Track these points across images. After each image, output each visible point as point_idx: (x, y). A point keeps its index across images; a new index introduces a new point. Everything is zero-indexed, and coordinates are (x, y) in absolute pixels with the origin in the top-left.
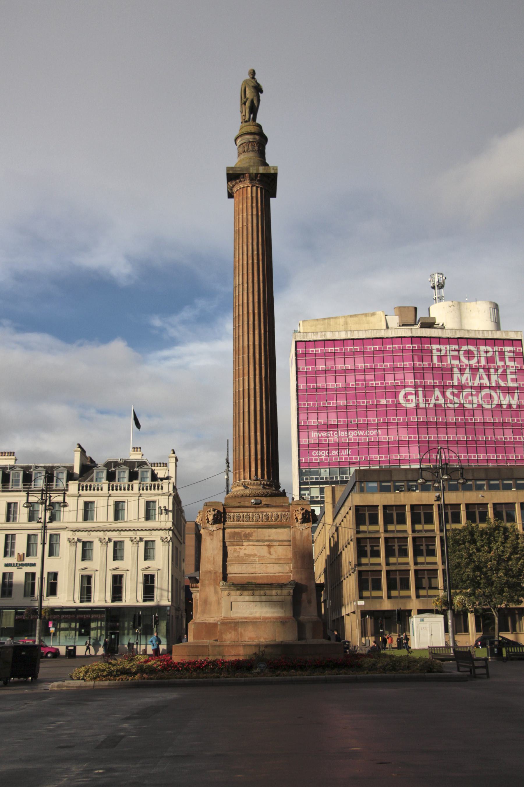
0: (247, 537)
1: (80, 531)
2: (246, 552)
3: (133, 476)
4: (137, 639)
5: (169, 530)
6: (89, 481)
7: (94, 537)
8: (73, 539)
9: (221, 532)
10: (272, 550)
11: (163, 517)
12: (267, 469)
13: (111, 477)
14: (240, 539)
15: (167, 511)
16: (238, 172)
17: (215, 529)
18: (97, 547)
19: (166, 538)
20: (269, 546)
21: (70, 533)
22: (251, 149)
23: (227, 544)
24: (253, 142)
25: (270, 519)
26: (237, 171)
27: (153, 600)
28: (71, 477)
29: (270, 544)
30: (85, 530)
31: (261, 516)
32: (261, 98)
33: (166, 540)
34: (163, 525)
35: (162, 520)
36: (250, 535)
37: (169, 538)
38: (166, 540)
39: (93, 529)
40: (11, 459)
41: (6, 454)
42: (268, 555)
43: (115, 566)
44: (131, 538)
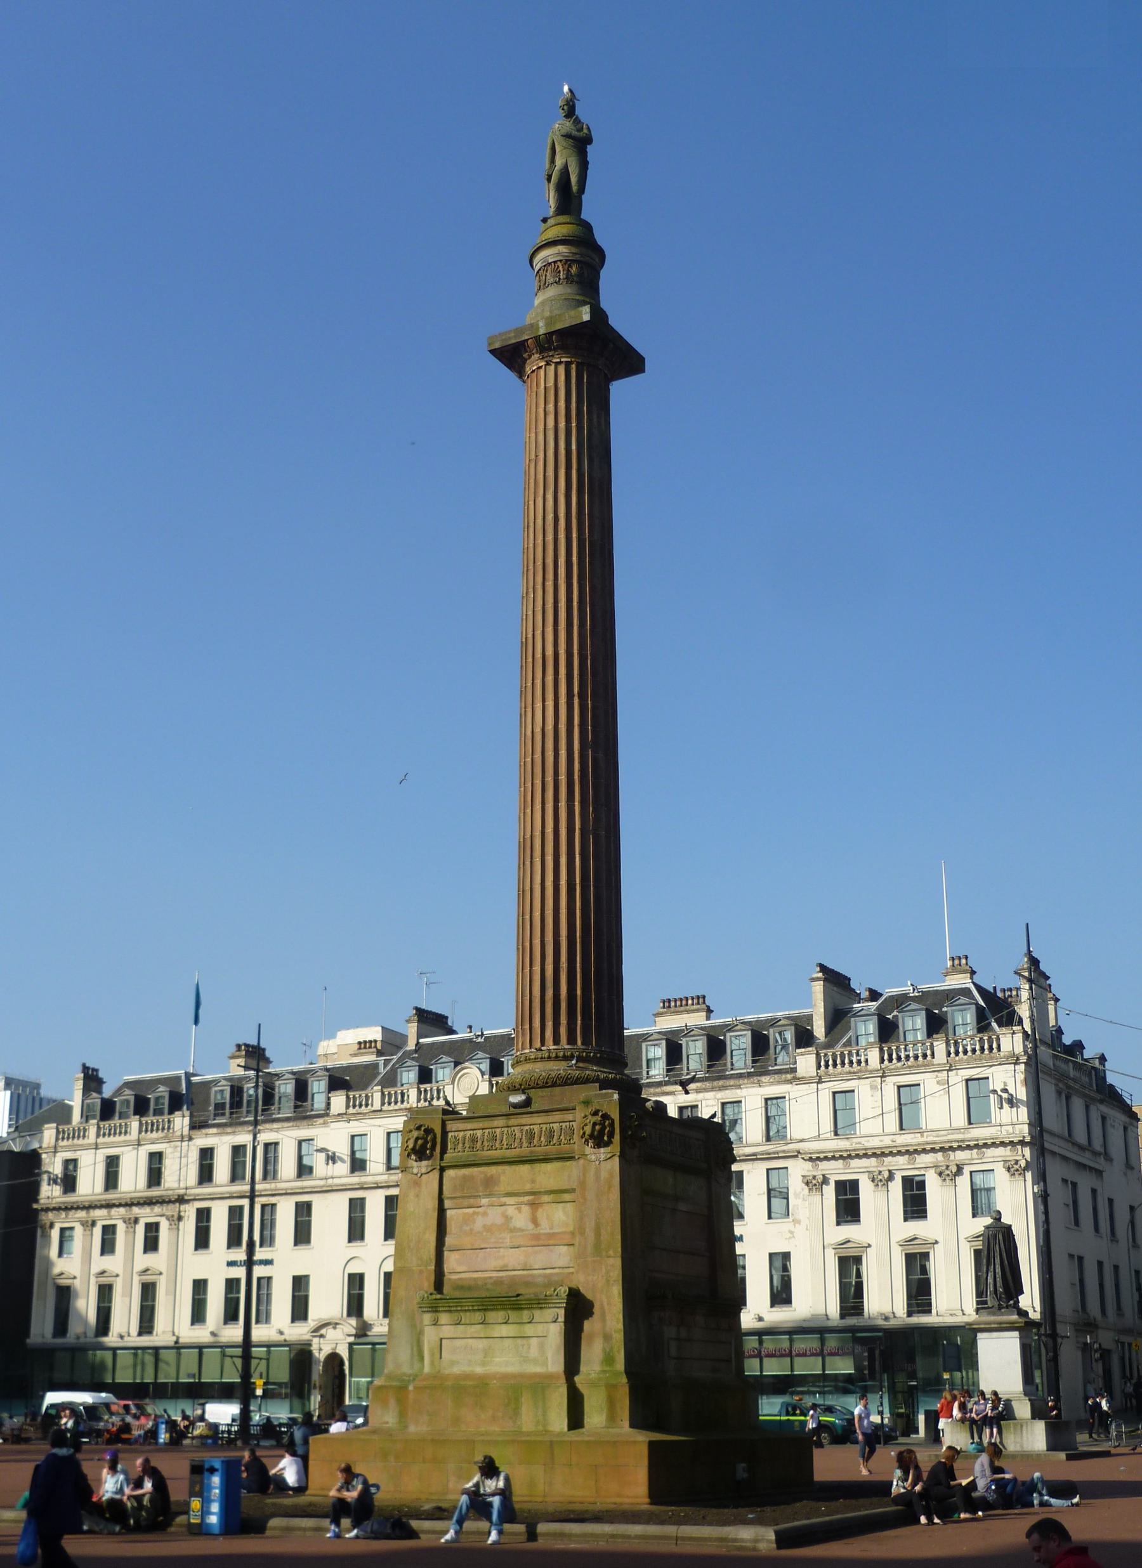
0: (489, 1183)
1: (826, 1158)
2: (489, 1221)
3: (936, 1024)
4: (882, 1405)
5: (1022, 1143)
6: (845, 1045)
7: (857, 1170)
8: (814, 1177)
9: (435, 1175)
10: (541, 1214)
11: (1007, 1114)
12: (582, 1019)
13: (887, 1031)
14: (469, 1195)
15: (1012, 1102)
16: (513, 341)
17: (424, 1170)
18: (867, 1194)
19: (1017, 1162)
20: (534, 1206)
21: (809, 1164)
22: (552, 280)
23: (447, 1204)
24: (555, 262)
25: (535, 1141)
26: (510, 338)
27: (930, 1311)
28: (804, 1038)
29: (535, 1198)
30: (928, 1147)
31: (518, 1135)
32: (590, 158)
33: (1016, 1167)
34: (1005, 1134)
35: (1004, 1121)
36: (489, 1182)
37: (1023, 1164)
38: (1016, 1167)
39: (919, 1148)
40: (697, 1011)
41: (690, 1002)
42: (531, 1226)
43: (841, 1238)
44: (936, 1167)
